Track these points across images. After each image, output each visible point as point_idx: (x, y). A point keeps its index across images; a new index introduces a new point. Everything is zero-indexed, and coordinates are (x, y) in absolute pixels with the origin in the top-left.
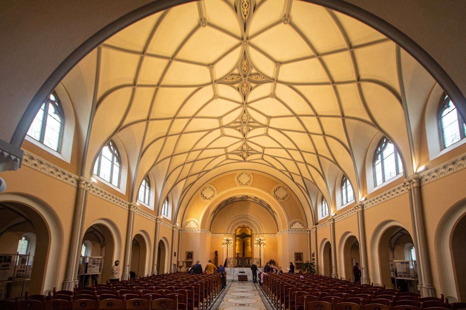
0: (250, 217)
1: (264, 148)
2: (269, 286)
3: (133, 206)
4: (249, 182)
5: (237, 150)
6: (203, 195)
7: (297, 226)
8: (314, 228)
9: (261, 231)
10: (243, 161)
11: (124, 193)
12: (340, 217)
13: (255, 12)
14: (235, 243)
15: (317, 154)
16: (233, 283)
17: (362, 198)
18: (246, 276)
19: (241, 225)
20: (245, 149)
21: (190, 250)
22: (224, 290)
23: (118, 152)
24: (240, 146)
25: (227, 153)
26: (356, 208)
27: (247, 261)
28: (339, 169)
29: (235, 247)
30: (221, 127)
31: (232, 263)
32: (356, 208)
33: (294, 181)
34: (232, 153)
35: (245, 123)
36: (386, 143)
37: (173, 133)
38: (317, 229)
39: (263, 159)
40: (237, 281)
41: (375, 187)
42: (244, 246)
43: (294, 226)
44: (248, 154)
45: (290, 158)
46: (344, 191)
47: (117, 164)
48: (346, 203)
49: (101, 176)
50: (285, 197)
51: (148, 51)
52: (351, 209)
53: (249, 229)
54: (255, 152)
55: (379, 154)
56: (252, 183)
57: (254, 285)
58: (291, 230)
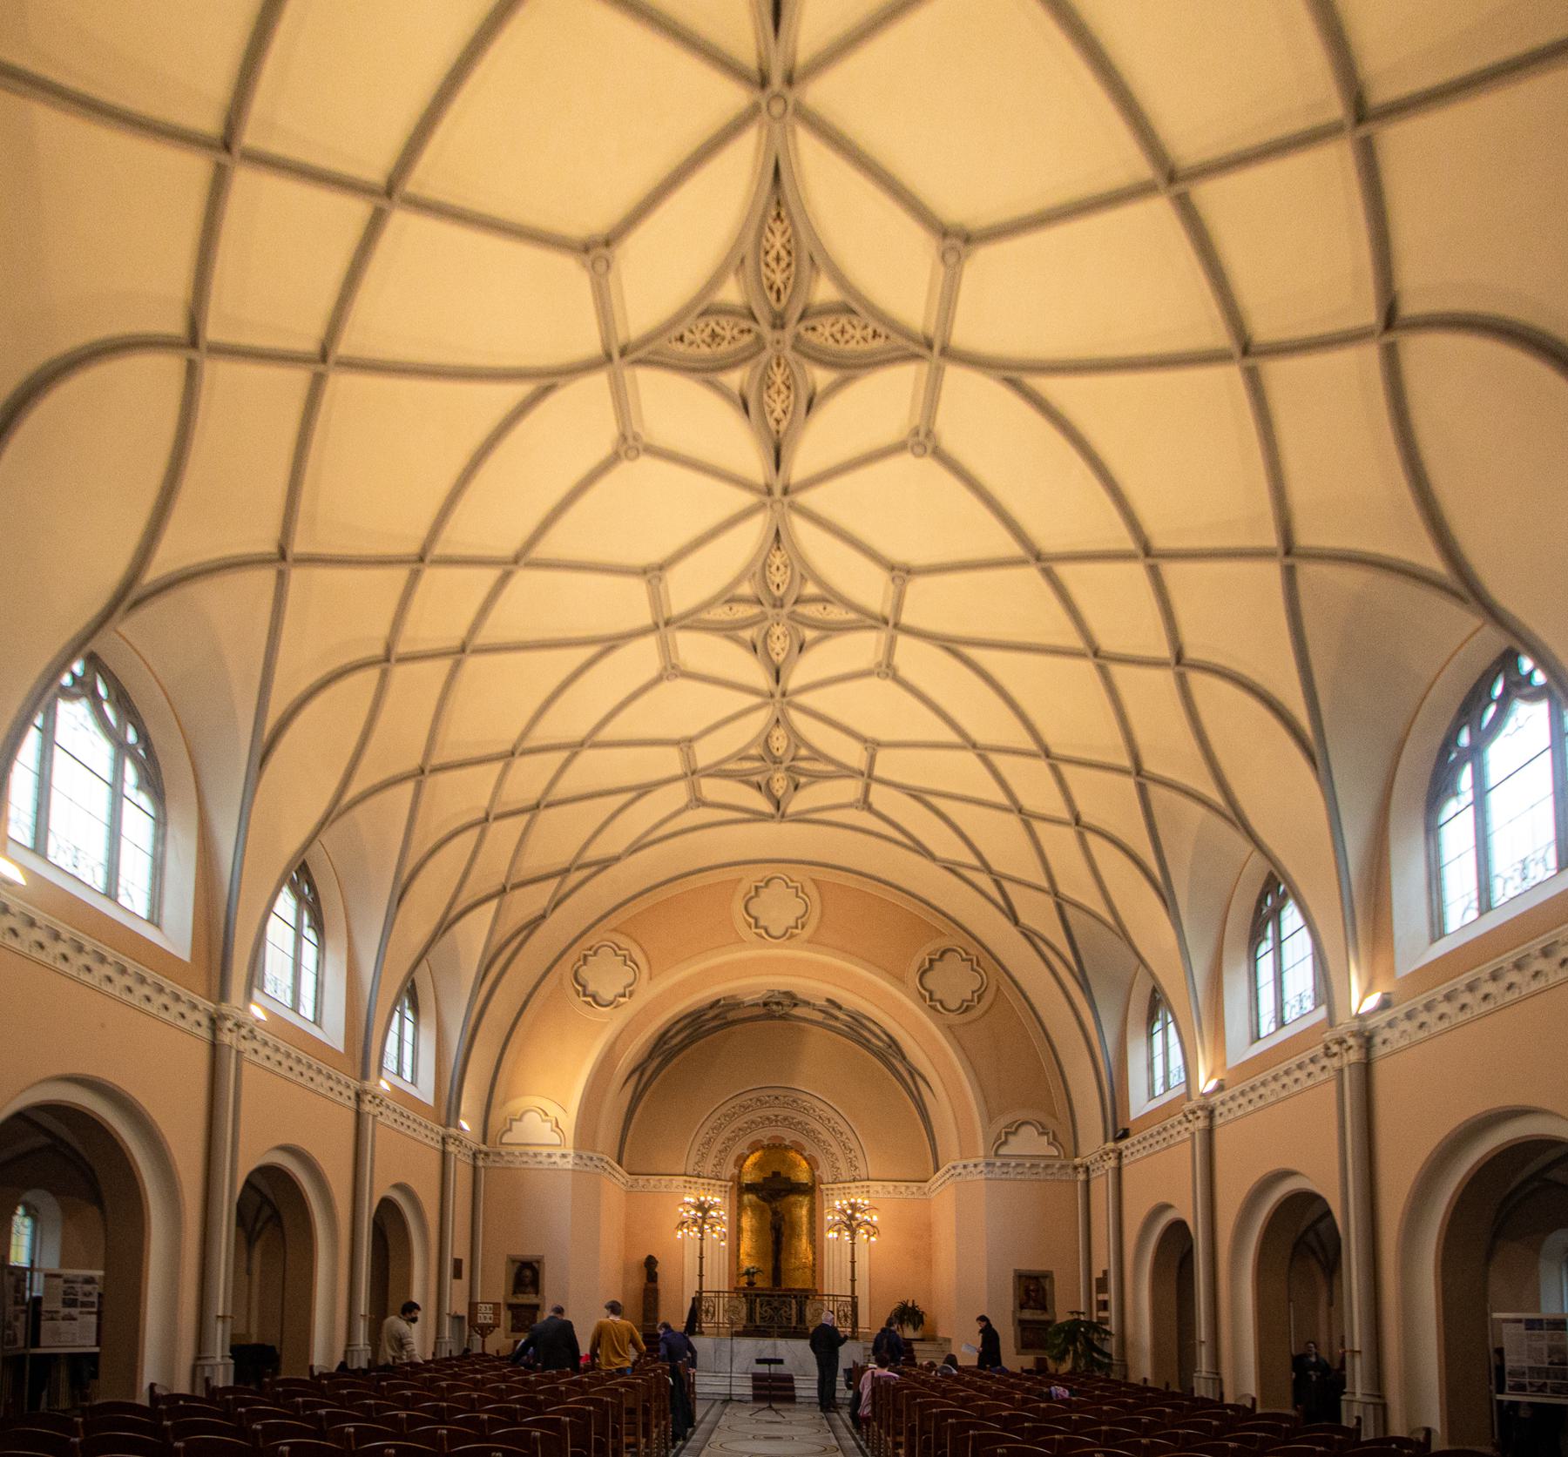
0: (805, 1097)
1: (873, 746)
2: (901, 1434)
3: (233, 1021)
4: (800, 923)
5: (743, 755)
6: (584, 987)
7: (1029, 1143)
8: (1111, 1155)
9: (856, 1168)
10: (772, 817)
11: (185, 954)
12: (1242, 1100)
13: (811, 414)
14: (739, 1220)
15: (1138, 770)
16: (727, 1410)
17: (1209, 1079)
18: (790, 1379)
19: (764, 1135)
20: (781, 752)
21: (528, 1252)
22: (683, 1447)
23: (143, 736)
24: (759, 736)
25: (693, 773)
26: (1335, 1049)
27: (791, 1309)
28: (1248, 847)
29: (739, 1239)
30: (661, 624)
31: (721, 1317)
32: (1335, 1049)
33: (1015, 920)
34: (717, 772)
35: (778, 603)
36: (1504, 703)
37: (422, 647)
38: (1125, 1161)
39: (866, 804)
40: (746, 1402)
41: (1433, 940)
42: (777, 1236)
43: (1016, 1146)
44: (793, 779)
45: (1000, 798)
46: (1266, 966)
47: (143, 800)
48: (1272, 1028)
49: (57, 850)
50: (972, 1000)
51: (343, 349)
52: (1305, 1057)
53: (801, 1154)
54: (831, 768)
55: (1466, 762)
56: (818, 929)
57: (825, 1422)
58: (998, 1164)
